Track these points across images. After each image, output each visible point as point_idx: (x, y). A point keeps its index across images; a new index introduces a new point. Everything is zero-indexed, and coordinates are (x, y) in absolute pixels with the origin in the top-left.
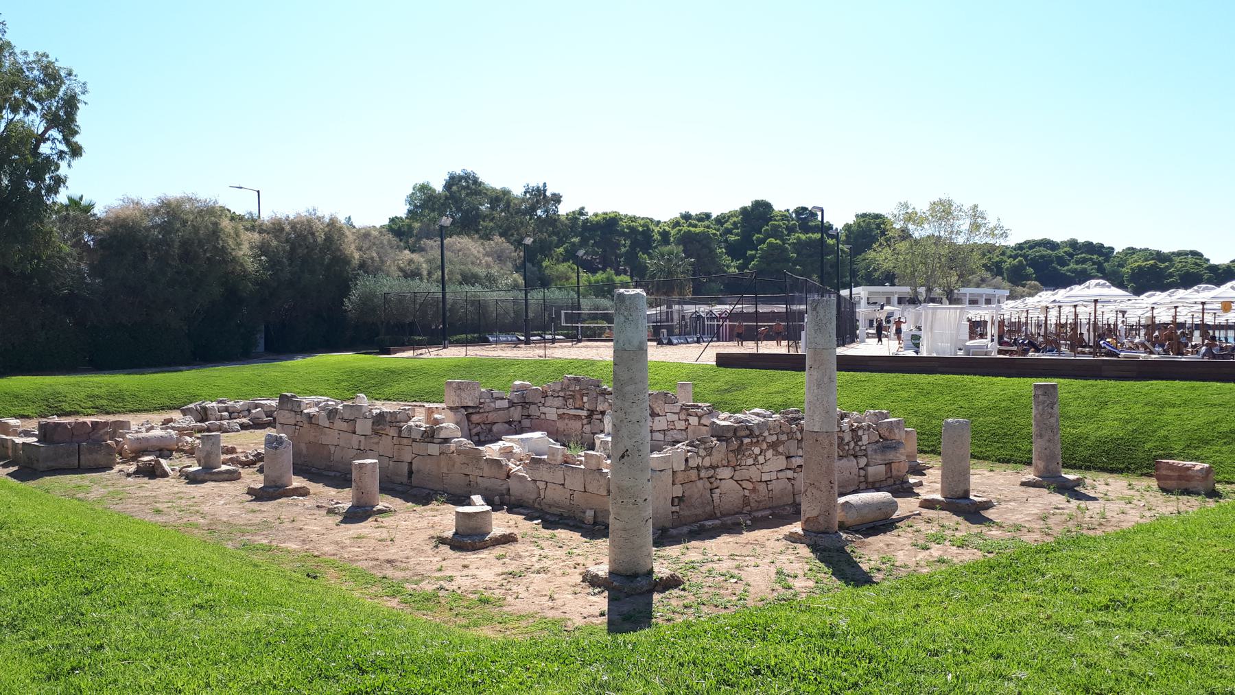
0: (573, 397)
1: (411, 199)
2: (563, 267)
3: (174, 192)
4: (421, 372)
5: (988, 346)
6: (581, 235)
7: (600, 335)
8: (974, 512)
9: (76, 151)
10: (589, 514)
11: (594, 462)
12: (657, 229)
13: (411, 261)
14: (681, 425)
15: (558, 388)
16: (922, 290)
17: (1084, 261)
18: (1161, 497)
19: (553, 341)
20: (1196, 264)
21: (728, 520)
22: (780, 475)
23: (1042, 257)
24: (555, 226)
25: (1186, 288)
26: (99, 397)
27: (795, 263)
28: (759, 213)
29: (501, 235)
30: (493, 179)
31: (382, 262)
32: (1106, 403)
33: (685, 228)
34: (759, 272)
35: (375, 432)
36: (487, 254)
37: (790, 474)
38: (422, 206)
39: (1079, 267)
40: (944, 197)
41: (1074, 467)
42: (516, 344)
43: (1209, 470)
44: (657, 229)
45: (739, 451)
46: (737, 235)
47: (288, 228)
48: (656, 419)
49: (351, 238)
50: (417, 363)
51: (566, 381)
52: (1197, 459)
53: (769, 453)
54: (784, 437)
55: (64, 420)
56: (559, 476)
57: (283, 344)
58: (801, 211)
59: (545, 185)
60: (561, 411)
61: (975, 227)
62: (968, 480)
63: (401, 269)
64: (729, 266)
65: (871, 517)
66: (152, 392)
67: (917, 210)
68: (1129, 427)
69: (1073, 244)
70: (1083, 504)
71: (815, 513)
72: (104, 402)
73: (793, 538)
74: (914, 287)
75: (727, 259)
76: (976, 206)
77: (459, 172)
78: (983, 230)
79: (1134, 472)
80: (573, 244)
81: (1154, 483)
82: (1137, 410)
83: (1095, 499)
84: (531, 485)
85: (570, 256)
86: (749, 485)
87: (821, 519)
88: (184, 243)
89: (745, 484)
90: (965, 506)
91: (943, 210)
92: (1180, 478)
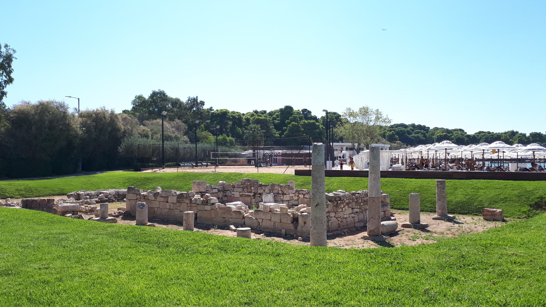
0: (247, 187)
1: (134, 102)
2: (204, 133)
3: (45, 98)
4: (160, 179)
5: (399, 166)
6: (211, 119)
7: (225, 163)
8: (424, 228)
9: (10, 80)
10: (283, 231)
11: (285, 210)
12: (244, 117)
13: (144, 130)
14: (296, 198)
15: (240, 184)
16: (356, 145)
17: (418, 133)
18: (486, 223)
19: (207, 166)
20: (462, 134)
21: (335, 233)
22: (350, 215)
23: (401, 131)
24: (201, 116)
25: (439, 143)
26: (20, 190)
27: (303, 132)
28: (287, 111)
29: (179, 119)
30: (172, 94)
31: (132, 131)
32: (457, 188)
33: (257, 117)
34: (287, 136)
35: (178, 202)
36: (172, 127)
37: (353, 215)
38: (139, 105)
39: (416, 135)
40: (365, 106)
41: (451, 213)
42: (193, 167)
43: (502, 212)
44: (244, 117)
45: (337, 206)
46: (278, 120)
47: (94, 115)
48: (285, 196)
49: (120, 120)
50: (154, 175)
51: (244, 181)
52: (497, 208)
53: (347, 207)
54: (351, 201)
55: (36, 199)
56: (268, 216)
57: (90, 167)
58: (304, 110)
59: (197, 97)
60: (241, 193)
61: (377, 118)
62: (419, 216)
63: (140, 134)
64: (275, 134)
65: (390, 230)
66: (44, 188)
67: (355, 111)
68: (468, 197)
69: (413, 125)
70: (461, 225)
71: (373, 228)
72: (24, 192)
73: (364, 238)
74: (353, 143)
75: (274, 131)
76: (378, 110)
77: (157, 90)
78: (381, 120)
79: (471, 214)
80: (207, 123)
81: (482, 218)
82: (469, 190)
83: (462, 223)
84: (255, 221)
85: (207, 128)
86: (339, 219)
87: (376, 231)
88: (51, 122)
89: (339, 219)
90: (417, 225)
91: (365, 112)
92: (491, 215)
